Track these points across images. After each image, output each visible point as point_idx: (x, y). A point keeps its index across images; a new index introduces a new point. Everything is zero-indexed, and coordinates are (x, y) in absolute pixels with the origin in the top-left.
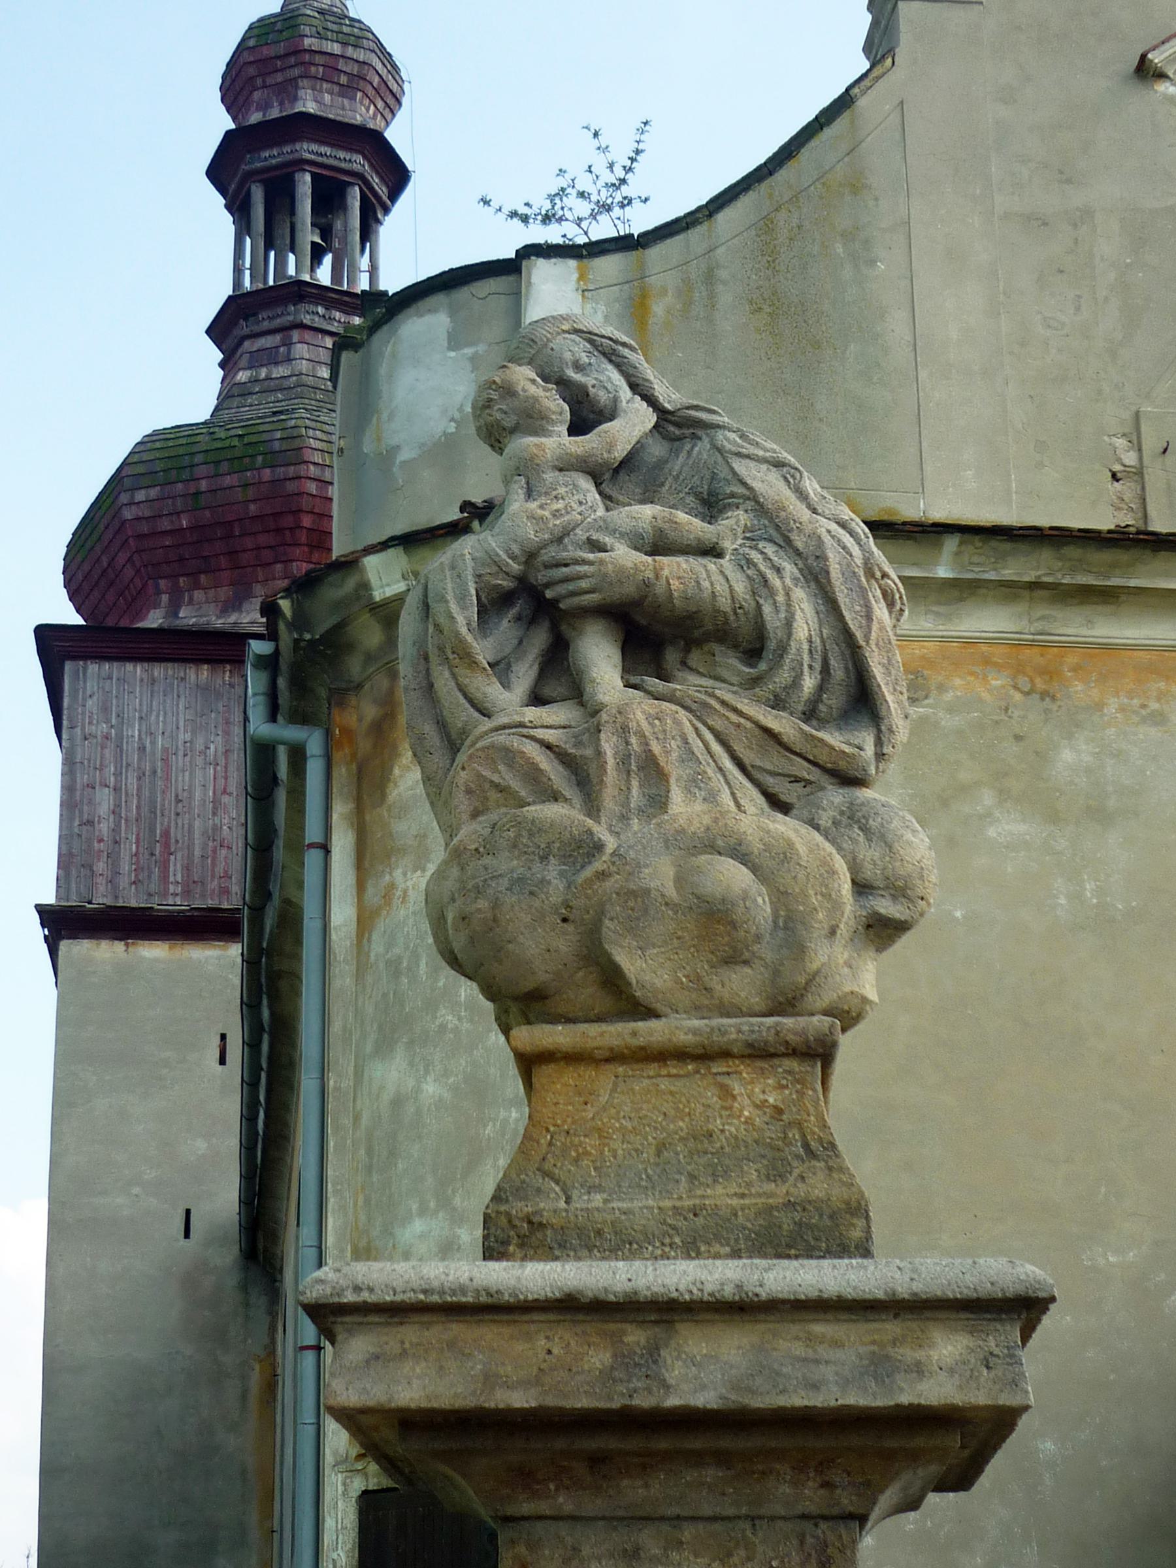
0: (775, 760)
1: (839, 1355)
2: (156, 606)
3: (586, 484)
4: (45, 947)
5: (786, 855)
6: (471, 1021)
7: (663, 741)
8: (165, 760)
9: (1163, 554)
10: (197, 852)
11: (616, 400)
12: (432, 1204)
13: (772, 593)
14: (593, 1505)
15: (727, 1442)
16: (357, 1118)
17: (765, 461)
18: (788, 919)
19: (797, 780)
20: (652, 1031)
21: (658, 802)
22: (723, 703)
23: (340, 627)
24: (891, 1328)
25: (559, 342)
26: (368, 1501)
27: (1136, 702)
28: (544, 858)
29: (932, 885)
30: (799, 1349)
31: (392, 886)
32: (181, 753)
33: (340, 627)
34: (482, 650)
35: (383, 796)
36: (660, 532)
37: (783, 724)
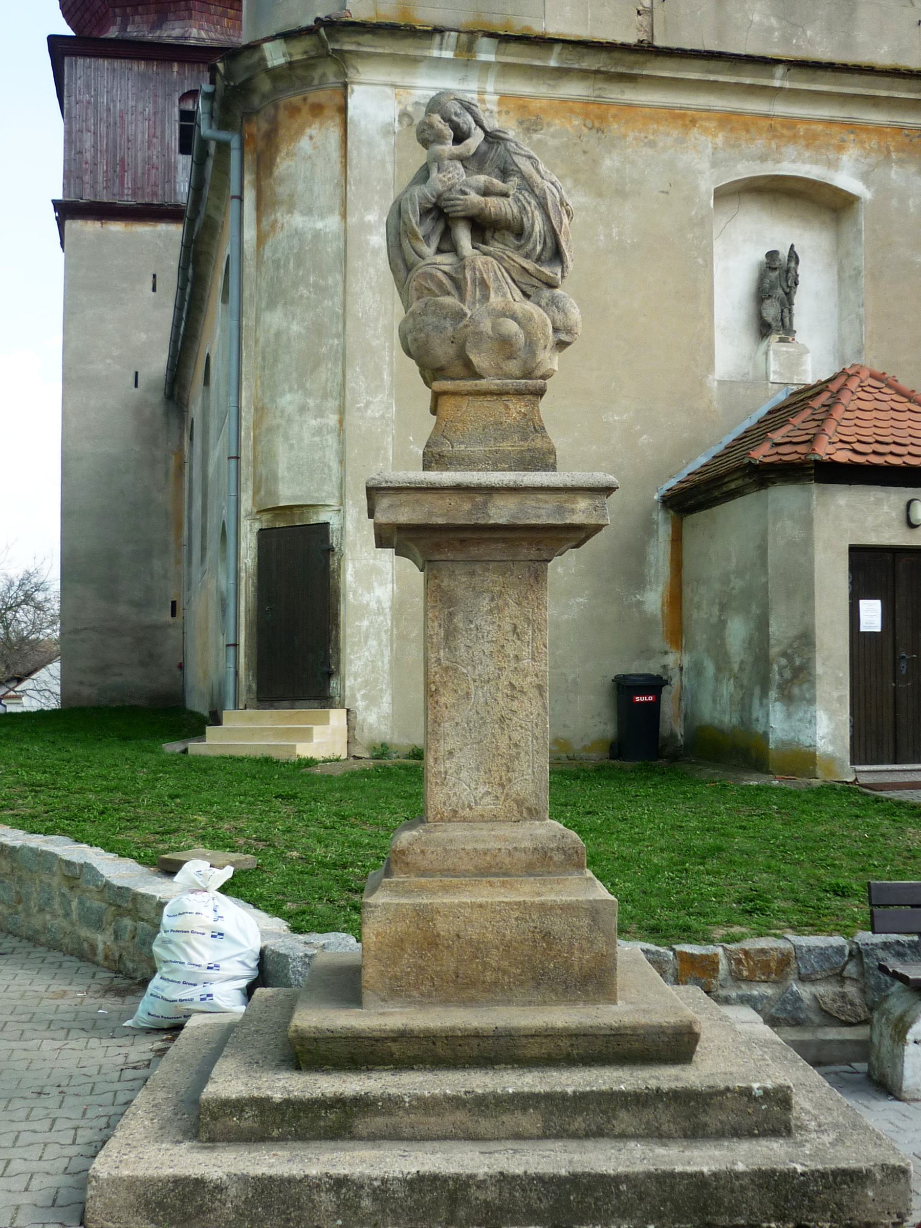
0: (526, 279)
1: (547, 506)
2: (114, 24)
3: (459, 165)
4: (56, 222)
5: (530, 319)
6: (315, 294)
7: (488, 273)
8: (121, 117)
9: (659, 58)
10: (140, 171)
11: (470, 129)
12: (296, 387)
13: (527, 213)
14: (460, 556)
15: (507, 535)
16: (257, 342)
17: (525, 156)
18: (530, 343)
19: (534, 286)
20: (483, 384)
21: (486, 297)
22: (509, 257)
23: (250, 79)
24: (564, 496)
25: (449, 104)
26: (263, 535)
27: (643, 135)
28: (445, 318)
29: (579, 329)
30: (533, 504)
31: (276, 221)
32: (130, 113)
33: (250, 79)
34: (420, 232)
35: (271, 173)
36: (487, 188)
37: (529, 265)
